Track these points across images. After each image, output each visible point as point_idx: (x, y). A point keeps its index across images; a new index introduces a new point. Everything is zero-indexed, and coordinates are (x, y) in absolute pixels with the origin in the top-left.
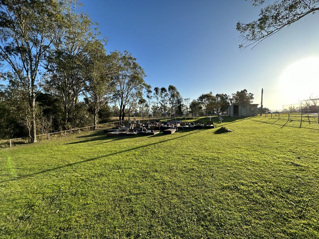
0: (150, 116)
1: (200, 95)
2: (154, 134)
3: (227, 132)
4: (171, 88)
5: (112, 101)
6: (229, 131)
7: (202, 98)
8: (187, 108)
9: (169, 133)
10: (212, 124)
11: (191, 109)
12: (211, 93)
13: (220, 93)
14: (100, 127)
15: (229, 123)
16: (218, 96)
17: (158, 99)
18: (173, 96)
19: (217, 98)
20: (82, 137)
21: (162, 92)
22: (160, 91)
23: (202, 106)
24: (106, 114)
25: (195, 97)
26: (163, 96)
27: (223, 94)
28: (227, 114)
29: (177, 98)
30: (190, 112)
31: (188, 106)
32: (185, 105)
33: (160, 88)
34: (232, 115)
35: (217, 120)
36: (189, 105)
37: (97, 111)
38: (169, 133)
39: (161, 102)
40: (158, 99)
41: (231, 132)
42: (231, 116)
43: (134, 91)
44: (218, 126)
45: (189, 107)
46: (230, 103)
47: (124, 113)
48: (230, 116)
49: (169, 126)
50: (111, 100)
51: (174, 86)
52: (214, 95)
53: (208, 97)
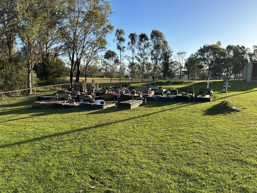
0: (127, 77)
1: (201, 45)
2: (103, 108)
3: (229, 113)
4: (155, 34)
5: (64, 52)
6: (234, 110)
7: (202, 51)
8: (181, 67)
9: (128, 107)
10: (209, 93)
11: (187, 68)
12: (219, 43)
13: (235, 44)
14: (37, 91)
15: (240, 92)
16: (230, 49)
17: (133, 51)
18: (157, 47)
19: (229, 52)
20: (6, 106)
21: (141, 40)
22: (137, 39)
23: (202, 63)
24: (56, 72)
25: (192, 50)
26: (141, 47)
27: (238, 46)
28: (243, 76)
29: (164, 50)
30: (185, 73)
31: (182, 64)
32: (179, 62)
33: (138, 33)
34: (249, 80)
35: (219, 87)
36: (184, 62)
37: (32, 66)
38: (128, 107)
39: (138, 56)
40: (133, 51)
41: (238, 111)
42: (247, 80)
43: (92, 37)
44: (216, 98)
45: (183, 65)
46: (249, 60)
47: (79, 72)
48: (245, 80)
49: (136, 95)
50: (62, 51)
51: (160, 31)
52: (224, 46)
53: (213, 49)
